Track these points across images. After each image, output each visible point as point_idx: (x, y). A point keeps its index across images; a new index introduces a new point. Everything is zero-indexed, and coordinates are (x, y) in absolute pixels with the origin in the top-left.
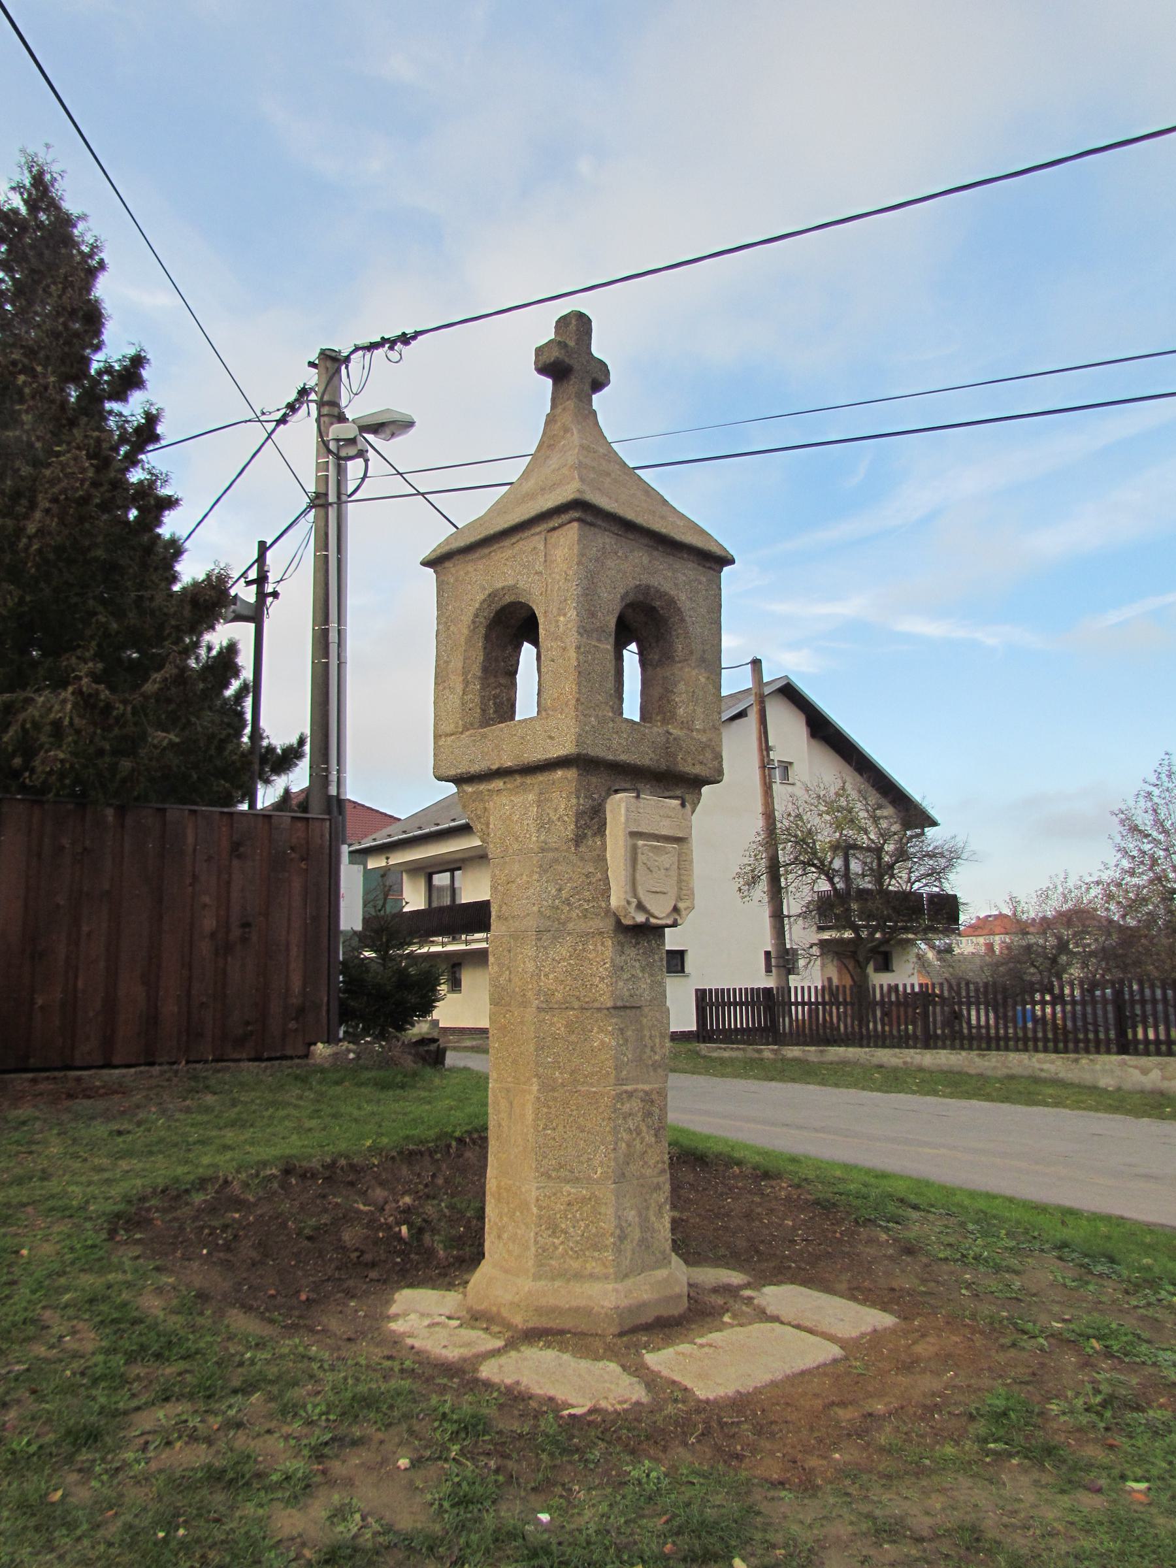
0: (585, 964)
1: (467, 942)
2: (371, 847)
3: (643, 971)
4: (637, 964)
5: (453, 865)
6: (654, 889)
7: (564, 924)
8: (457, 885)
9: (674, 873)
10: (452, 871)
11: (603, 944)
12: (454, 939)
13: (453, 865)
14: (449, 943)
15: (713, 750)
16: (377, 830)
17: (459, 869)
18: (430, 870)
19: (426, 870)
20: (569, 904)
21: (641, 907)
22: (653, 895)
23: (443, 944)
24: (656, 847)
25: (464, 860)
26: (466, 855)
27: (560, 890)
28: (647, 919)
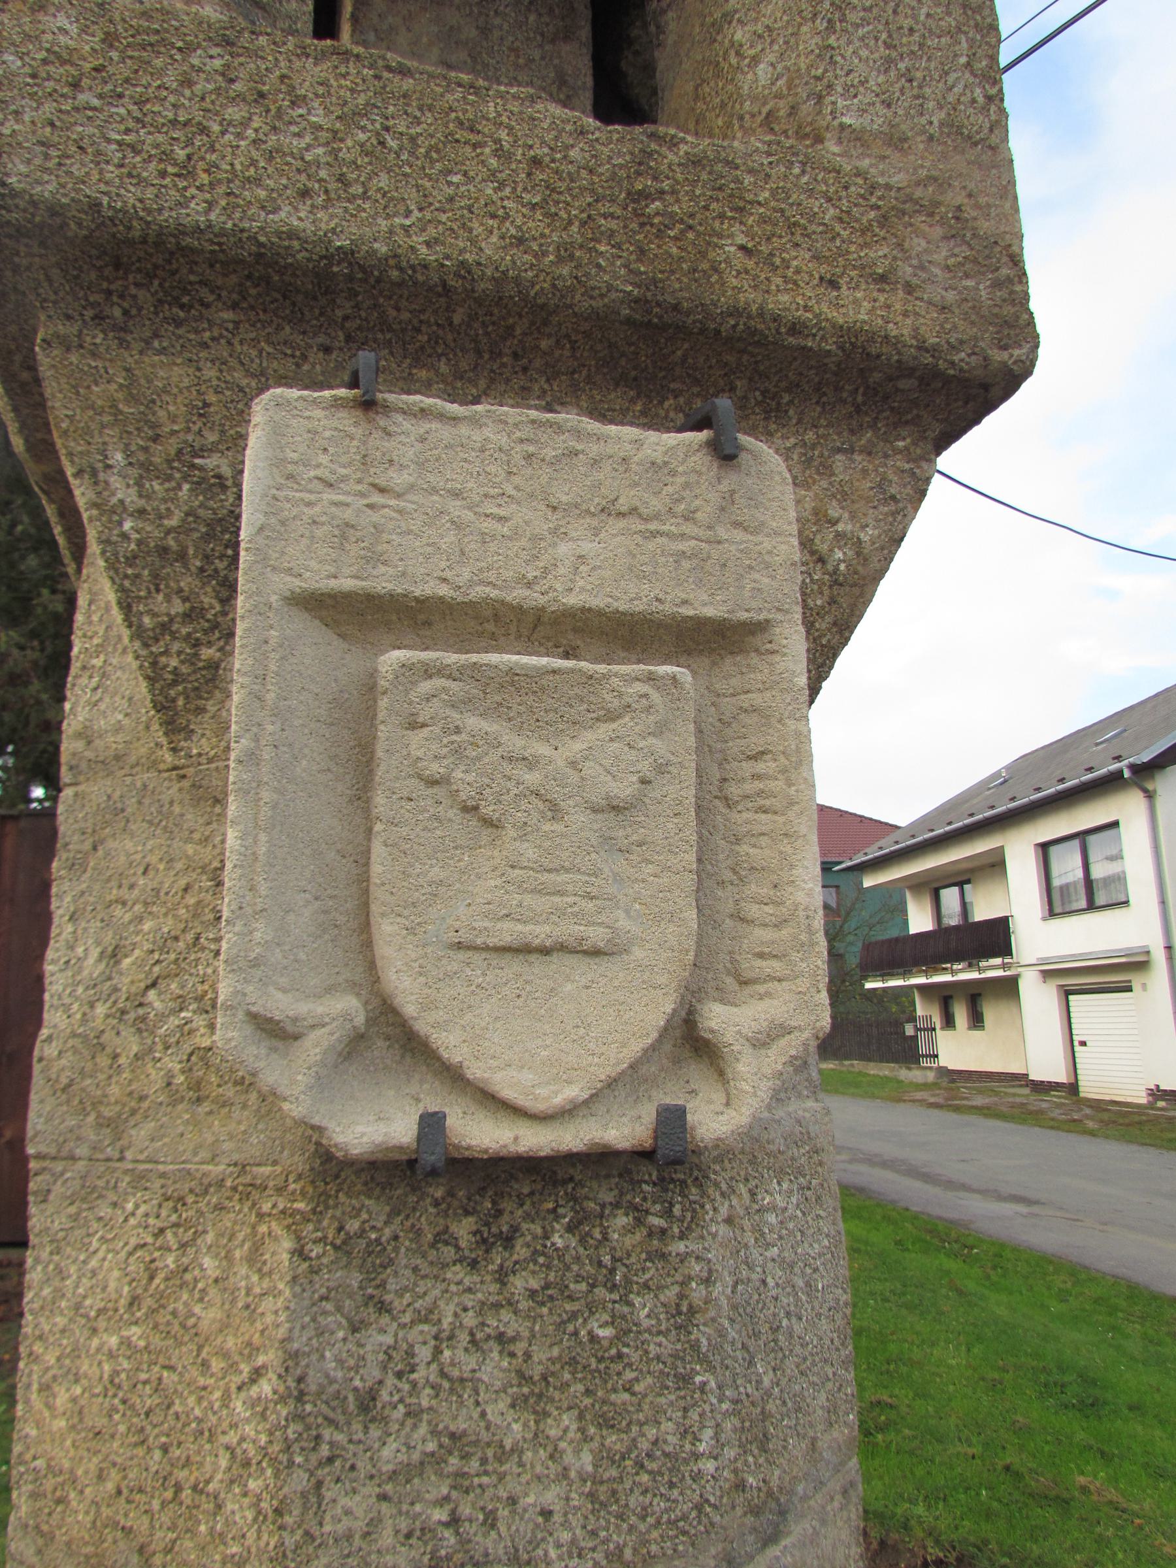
0: (183, 1356)
1: (979, 970)
2: (863, 862)
3: (533, 1395)
4: (493, 1368)
5: (962, 877)
6: (508, 932)
7: (115, 1126)
8: (967, 900)
9: (672, 829)
10: (960, 884)
11: (254, 1258)
12: (970, 965)
13: (962, 877)
14: (961, 971)
15: (958, 227)
16: (869, 844)
17: (968, 882)
18: (936, 885)
19: (931, 887)
20: (142, 1026)
21: (392, 1039)
22: (514, 966)
23: (953, 973)
24: (513, 678)
25: (972, 871)
26: (976, 863)
27: (114, 955)
28: (432, 1124)
